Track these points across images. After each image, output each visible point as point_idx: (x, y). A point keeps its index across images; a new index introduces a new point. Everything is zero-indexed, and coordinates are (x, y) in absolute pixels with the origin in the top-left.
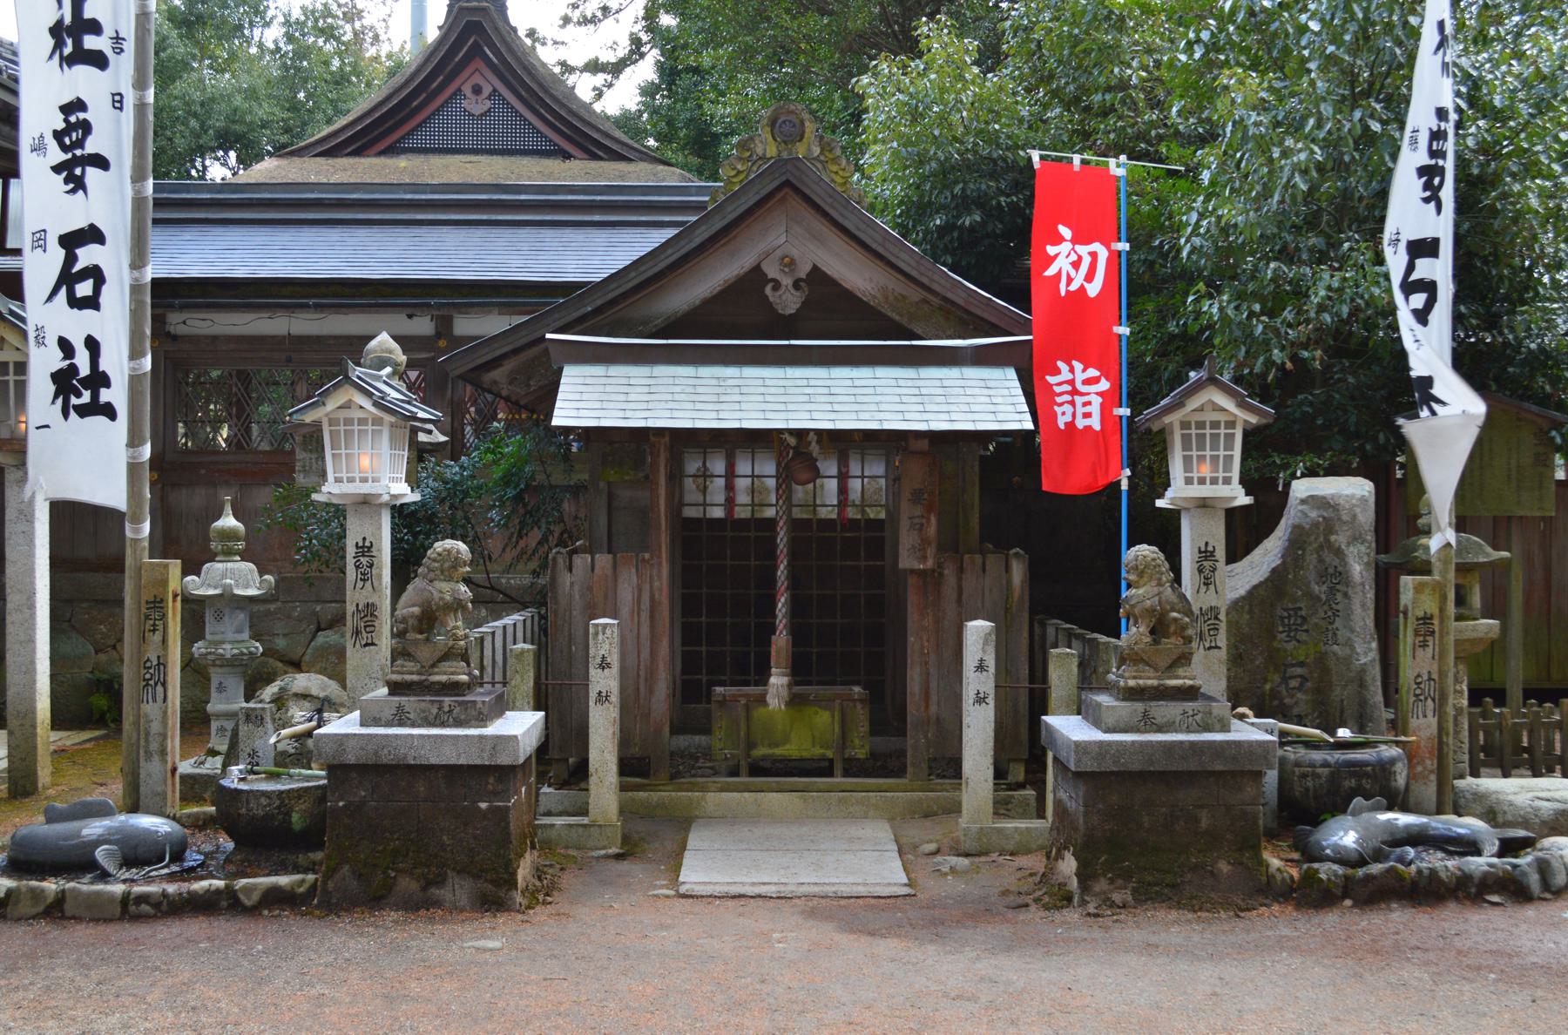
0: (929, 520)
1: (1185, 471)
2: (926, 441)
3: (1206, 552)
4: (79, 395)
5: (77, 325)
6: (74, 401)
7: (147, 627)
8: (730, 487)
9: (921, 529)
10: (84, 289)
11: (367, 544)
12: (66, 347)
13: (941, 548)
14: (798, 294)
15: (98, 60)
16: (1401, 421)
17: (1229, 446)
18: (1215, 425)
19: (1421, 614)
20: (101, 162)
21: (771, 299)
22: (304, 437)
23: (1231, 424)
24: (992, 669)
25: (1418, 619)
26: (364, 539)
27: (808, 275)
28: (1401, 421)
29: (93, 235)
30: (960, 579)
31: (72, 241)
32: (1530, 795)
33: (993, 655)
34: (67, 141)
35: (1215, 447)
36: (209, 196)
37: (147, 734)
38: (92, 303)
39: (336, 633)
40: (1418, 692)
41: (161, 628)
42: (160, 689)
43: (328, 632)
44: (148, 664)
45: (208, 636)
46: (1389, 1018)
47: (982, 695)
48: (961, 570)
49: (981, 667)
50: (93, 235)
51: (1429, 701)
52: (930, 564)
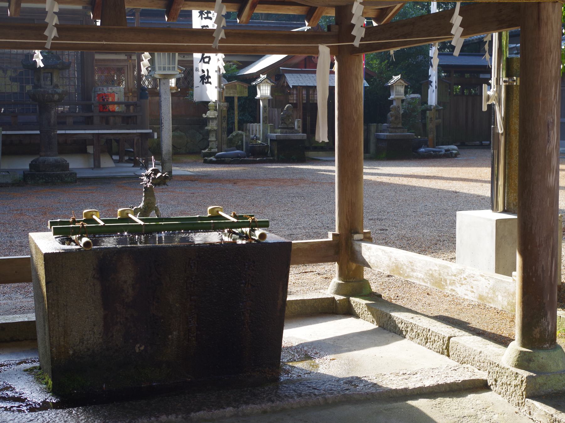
4: (205, 80)
6: (205, 81)
12: (203, 71)
16: (58, 36)
28: (58, 36)
36: (269, 45)
38: (208, 63)
45: (210, 126)
46: (299, 386)
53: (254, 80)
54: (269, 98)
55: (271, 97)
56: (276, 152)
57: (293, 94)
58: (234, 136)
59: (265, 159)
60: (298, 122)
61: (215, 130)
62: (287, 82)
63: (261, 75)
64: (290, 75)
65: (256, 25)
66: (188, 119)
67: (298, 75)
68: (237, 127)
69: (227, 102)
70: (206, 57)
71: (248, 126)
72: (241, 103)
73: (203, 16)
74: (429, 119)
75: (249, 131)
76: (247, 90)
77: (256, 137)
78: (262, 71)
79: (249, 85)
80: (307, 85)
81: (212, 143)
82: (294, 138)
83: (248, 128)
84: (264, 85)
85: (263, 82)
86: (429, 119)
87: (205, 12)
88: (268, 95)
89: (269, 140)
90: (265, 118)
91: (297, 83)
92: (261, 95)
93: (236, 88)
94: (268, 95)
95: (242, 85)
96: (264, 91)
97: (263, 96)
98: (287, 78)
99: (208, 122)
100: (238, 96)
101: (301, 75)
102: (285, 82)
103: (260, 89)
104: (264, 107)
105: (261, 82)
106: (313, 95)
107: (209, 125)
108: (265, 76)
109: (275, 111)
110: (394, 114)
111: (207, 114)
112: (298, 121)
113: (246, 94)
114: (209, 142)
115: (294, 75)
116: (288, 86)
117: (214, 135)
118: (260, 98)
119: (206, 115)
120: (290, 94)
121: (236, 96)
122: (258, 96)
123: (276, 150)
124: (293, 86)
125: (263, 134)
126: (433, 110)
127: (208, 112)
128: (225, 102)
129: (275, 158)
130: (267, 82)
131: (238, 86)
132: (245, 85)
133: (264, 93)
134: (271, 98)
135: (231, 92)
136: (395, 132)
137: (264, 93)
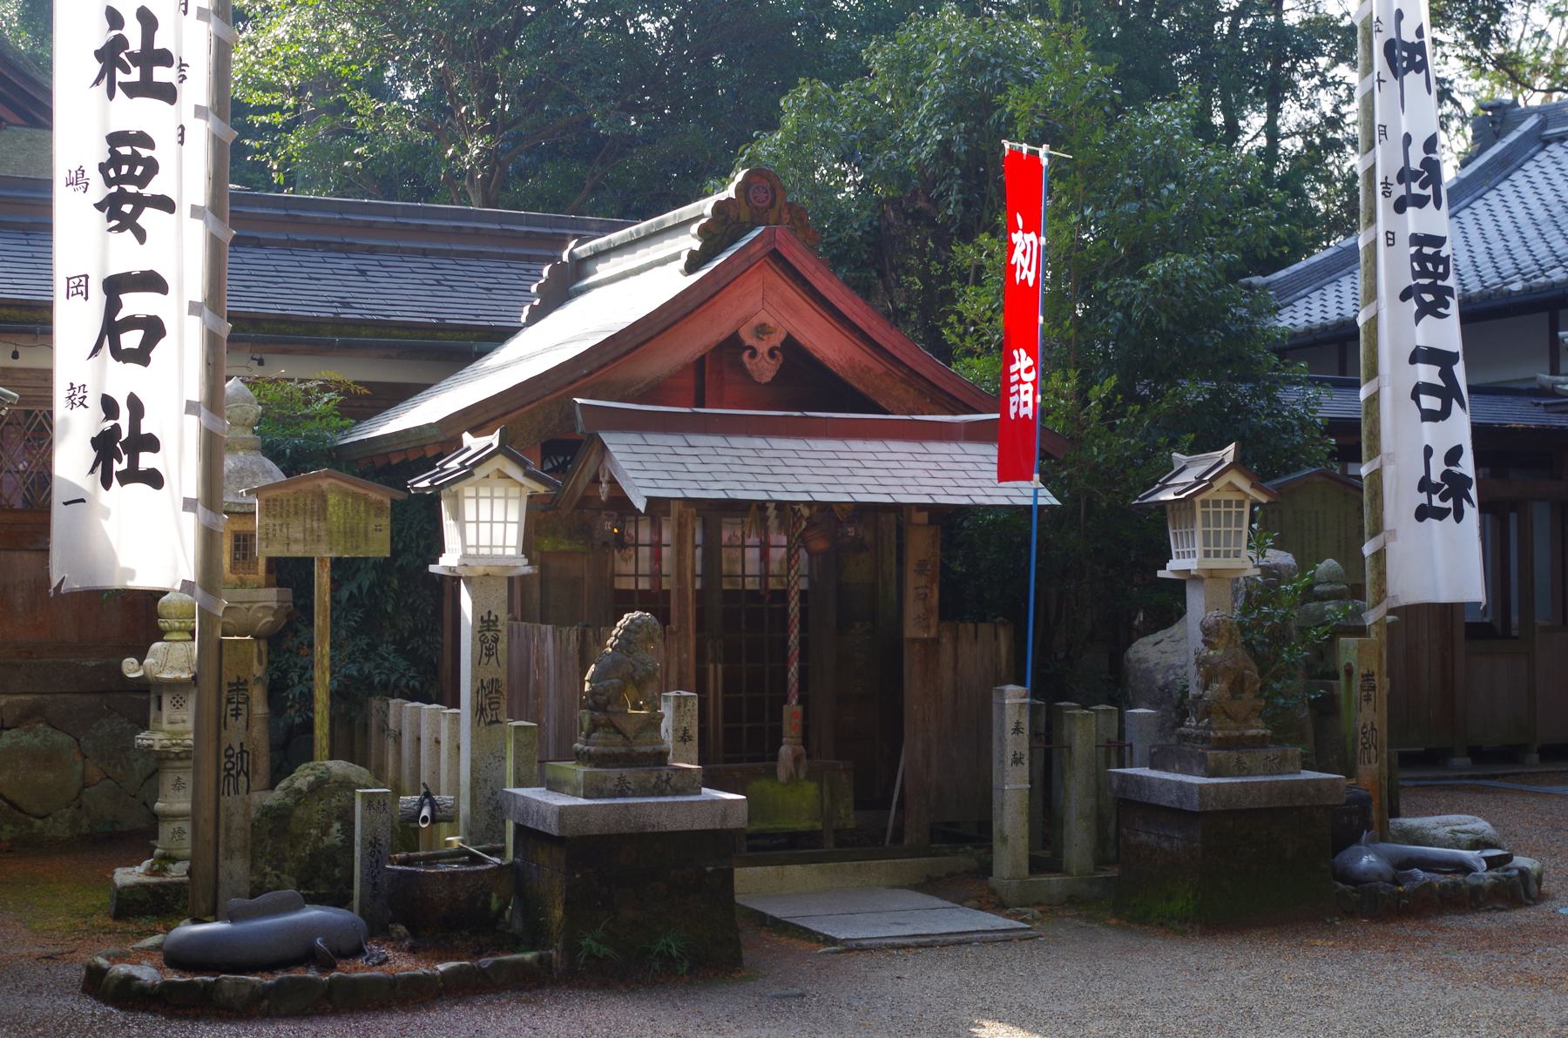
0: (931, 589)
1: (1205, 546)
2: (925, 514)
3: (489, 620)
5: (121, 380)
7: (229, 712)
8: (657, 557)
9: (925, 599)
10: (131, 339)
11: (492, 618)
12: (109, 407)
13: (943, 616)
14: (773, 362)
15: (167, 93)
17: (1239, 523)
18: (1228, 503)
19: (1365, 672)
20: (165, 204)
21: (748, 366)
22: (268, 500)
23: (1240, 504)
24: (1027, 732)
25: (1363, 676)
26: (490, 613)
27: (782, 344)
29: (151, 282)
30: (955, 649)
31: (116, 286)
32: (1448, 829)
33: (1028, 718)
34: (112, 173)
35: (1228, 524)
37: (228, 829)
38: (141, 356)
39: (27, 731)
40: (1364, 740)
41: (244, 712)
42: (242, 778)
43: (14, 732)
44: (230, 752)
45: (165, 726)
47: (1018, 756)
48: (956, 639)
49: (1017, 730)
50: (151, 282)
51: (1373, 748)
52: (933, 633)
53: (425, 464)
54: (514, 573)
55: (523, 567)
56: (558, 913)
57: (637, 545)
58: (299, 791)
59: (486, 961)
60: (678, 707)
61: (186, 755)
62: (613, 482)
63: (467, 438)
64: (633, 438)
65: (446, 223)
66: (92, 663)
67: (674, 440)
68: (326, 729)
69: (280, 584)
70: (132, 323)
71: (392, 712)
72: (360, 587)
73: (120, 76)
74: (1357, 681)
75: (398, 737)
76: (385, 522)
77: (433, 804)
78: (476, 418)
79: (399, 495)
80: (732, 495)
81: (176, 825)
82: (671, 827)
83: (392, 725)
84: (484, 492)
85: (480, 473)
86: (1357, 681)
87: (130, 55)
88: (511, 552)
89: (510, 826)
90: (487, 693)
91: (720, 485)
92: (465, 556)
93: (322, 513)
94: (511, 552)
95: (355, 496)
96: (484, 528)
97: (477, 556)
98: (617, 457)
99: (153, 707)
100: (334, 555)
101: (694, 439)
102: (604, 479)
103: (457, 515)
104: (486, 623)
105: (470, 474)
106: (738, 552)
107: (158, 720)
108: (494, 439)
109: (543, 640)
110: (1228, 663)
111: (148, 661)
112: (680, 703)
113: (379, 546)
114: (156, 818)
115: (652, 438)
116: (620, 502)
117: (188, 778)
118: (462, 572)
119: (141, 663)
120: (621, 543)
121: (324, 552)
122: (449, 560)
123: (559, 900)
124: (651, 501)
125: (472, 789)
126: (1373, 636)
127: (157, 645)
128: (268, 585)
129: (553, 952)
130: (504, 476)
131: (332, 499)
132: (373, 496)
133: (484, 540)
134: (528, 570)
135: (296, 531)
136: (1241, 770)
137: (484, 540)
